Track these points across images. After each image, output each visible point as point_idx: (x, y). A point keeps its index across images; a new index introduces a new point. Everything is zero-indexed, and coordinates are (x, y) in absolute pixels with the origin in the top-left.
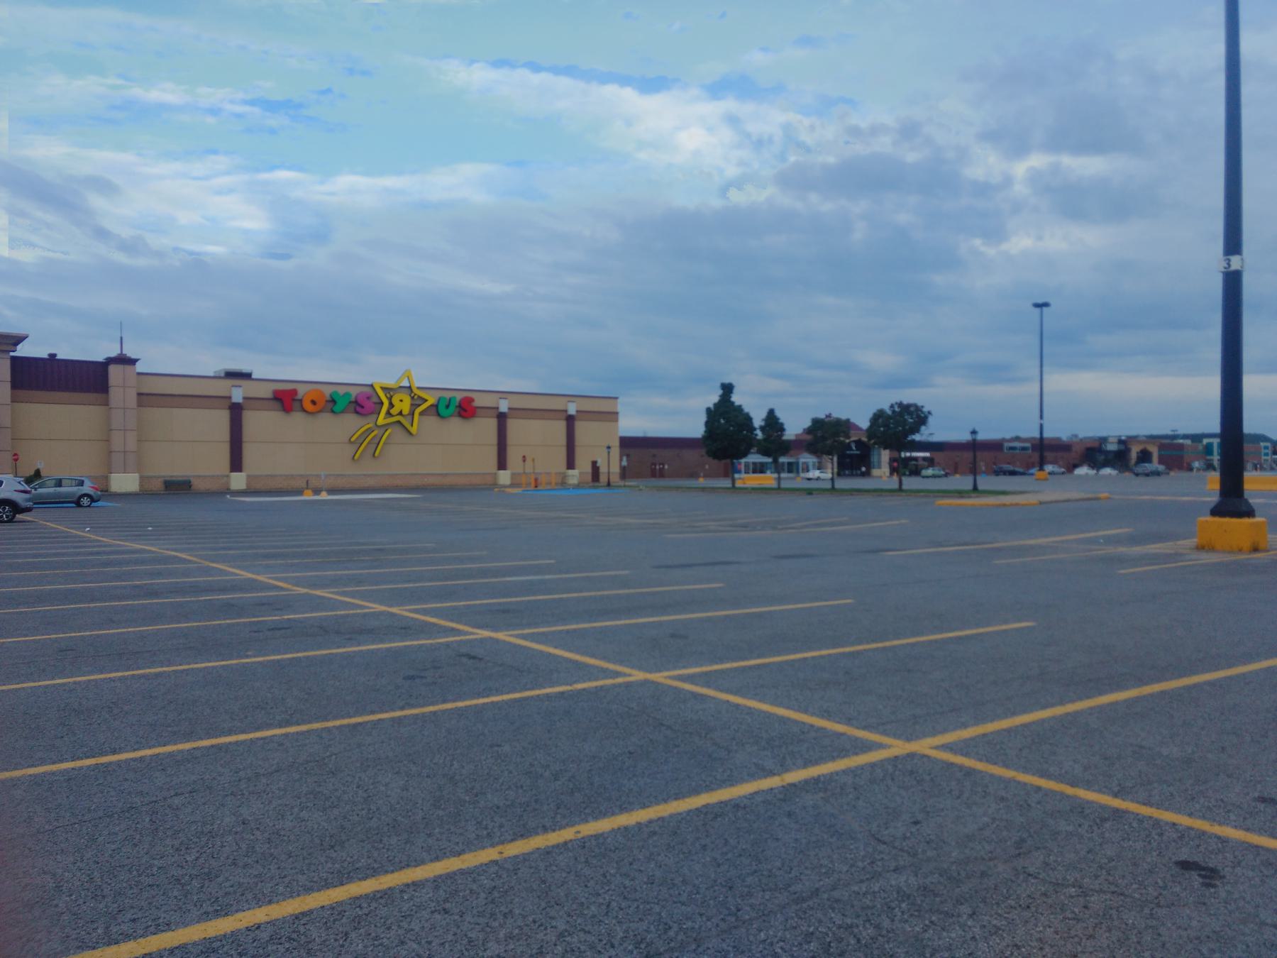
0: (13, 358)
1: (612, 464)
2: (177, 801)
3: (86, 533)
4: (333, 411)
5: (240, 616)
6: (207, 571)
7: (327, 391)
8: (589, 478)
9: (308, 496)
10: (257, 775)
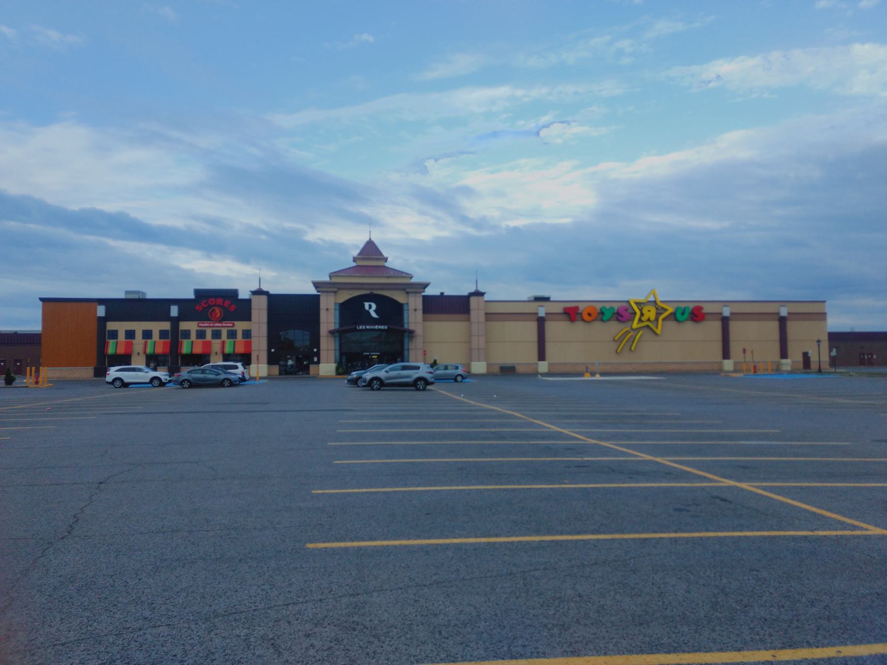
0: (424, 296)
1: (822, 355)
2: (537, 573)
3: (461, 398)
4: (602, 320)
5: (556, 456)
6: (532, 425)
7: (598, 306)
8: (801, 366)
9: (587, 377)
10: (583, 565)
